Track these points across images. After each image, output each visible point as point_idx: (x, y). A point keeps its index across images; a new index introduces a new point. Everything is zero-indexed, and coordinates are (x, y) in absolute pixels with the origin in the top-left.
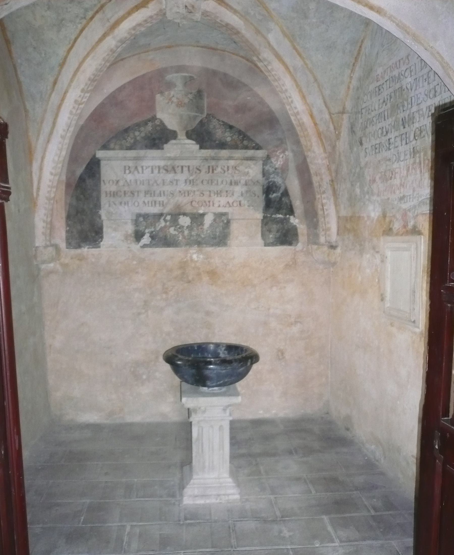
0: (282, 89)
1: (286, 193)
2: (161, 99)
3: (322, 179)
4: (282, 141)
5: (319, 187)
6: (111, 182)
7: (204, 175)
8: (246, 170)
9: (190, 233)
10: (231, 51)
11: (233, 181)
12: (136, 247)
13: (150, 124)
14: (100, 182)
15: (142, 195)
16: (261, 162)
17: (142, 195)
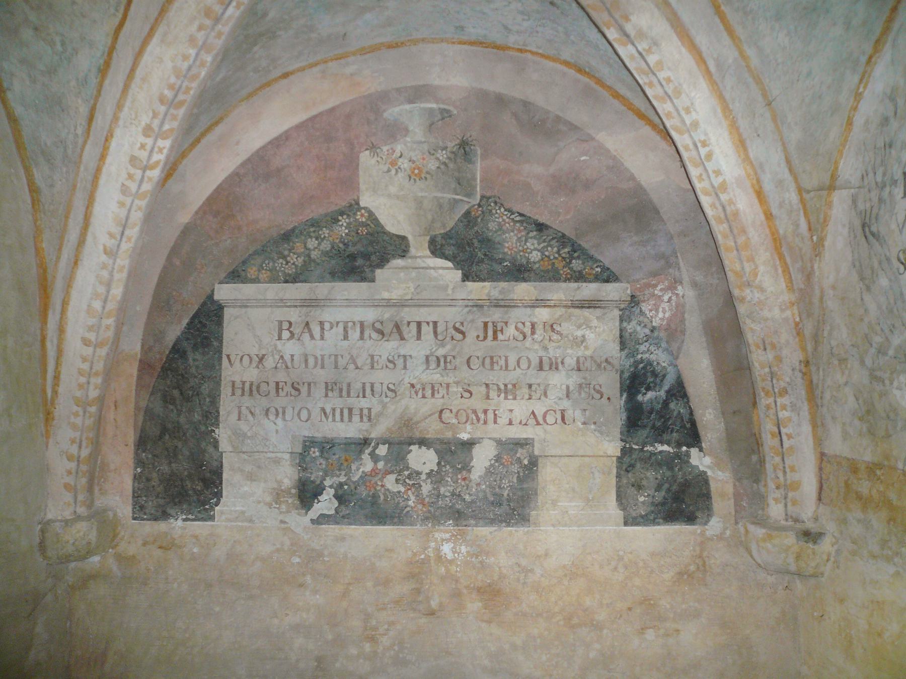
0: (683, 122)
1: (679, 391)
2: (373, 161)
3: (779, 359)
4: (667, 261)
5: (769, 379)
6: (246, 360)
7: (472, 346)
8: (579, 333)
9: (437, 489)
10: (540, 51)
11: (546, 361)
12: (300, 521)
13: (344, 221)
14: (220, 359)
15: (318, 392)
16: (617, 313)
17: (318, 392)
